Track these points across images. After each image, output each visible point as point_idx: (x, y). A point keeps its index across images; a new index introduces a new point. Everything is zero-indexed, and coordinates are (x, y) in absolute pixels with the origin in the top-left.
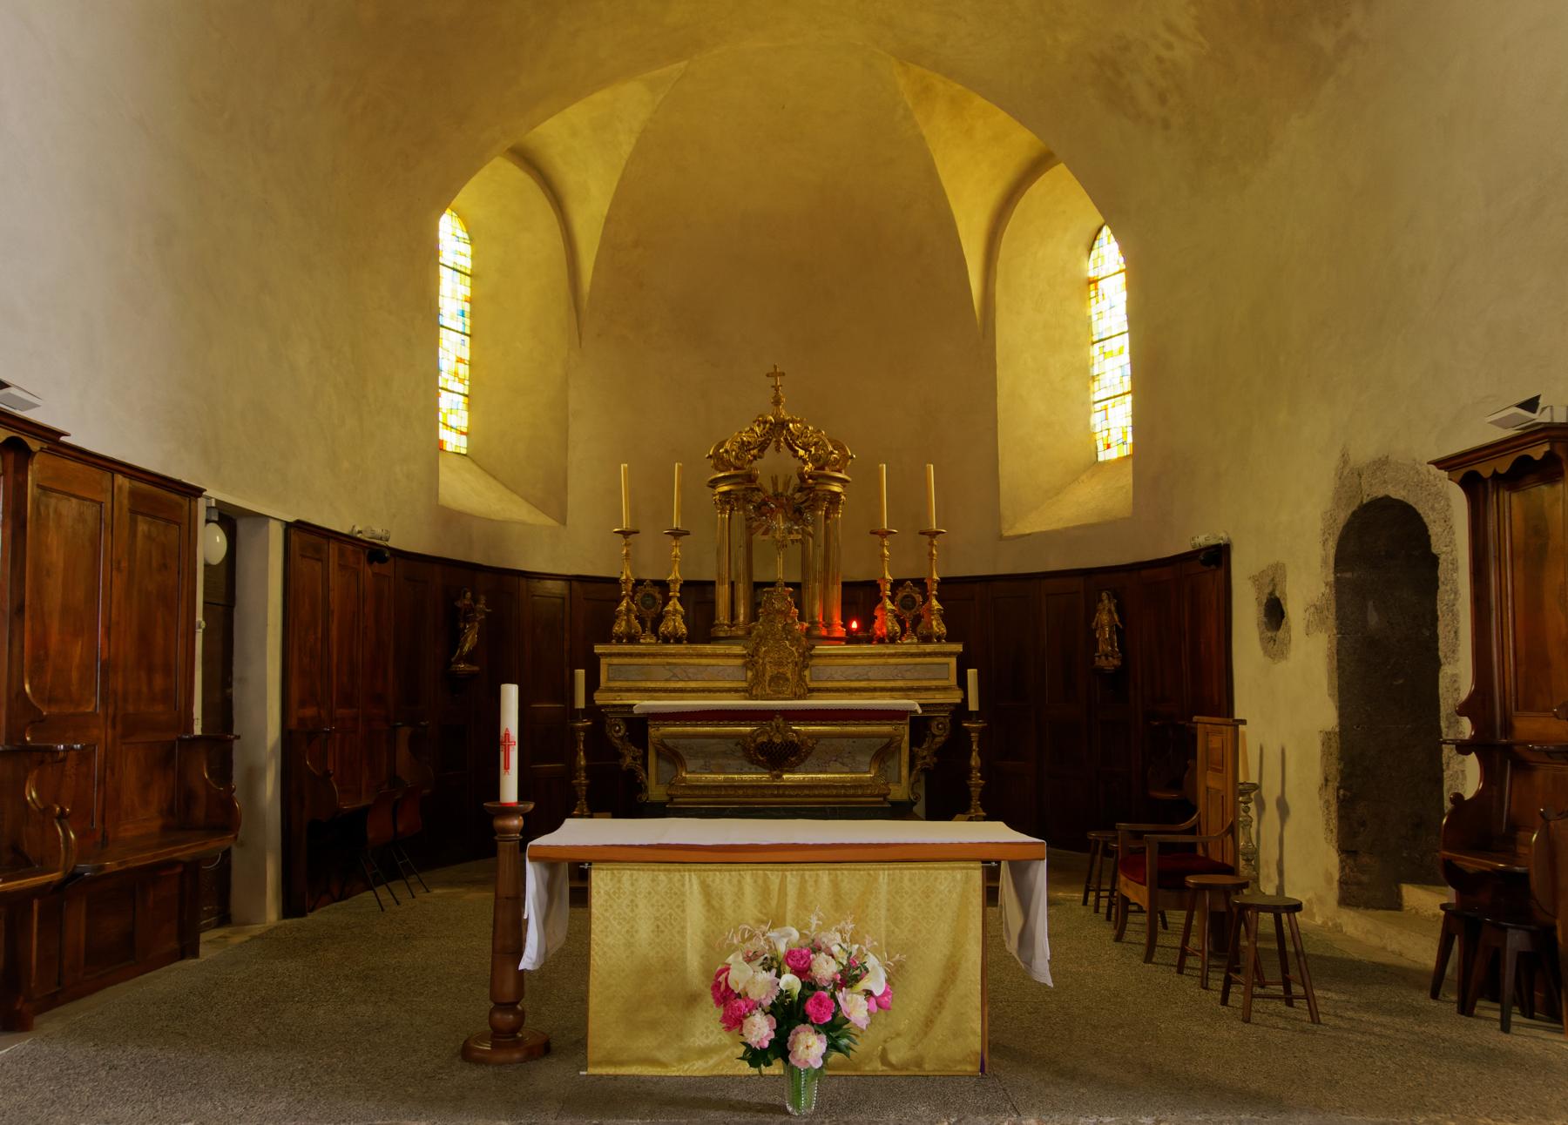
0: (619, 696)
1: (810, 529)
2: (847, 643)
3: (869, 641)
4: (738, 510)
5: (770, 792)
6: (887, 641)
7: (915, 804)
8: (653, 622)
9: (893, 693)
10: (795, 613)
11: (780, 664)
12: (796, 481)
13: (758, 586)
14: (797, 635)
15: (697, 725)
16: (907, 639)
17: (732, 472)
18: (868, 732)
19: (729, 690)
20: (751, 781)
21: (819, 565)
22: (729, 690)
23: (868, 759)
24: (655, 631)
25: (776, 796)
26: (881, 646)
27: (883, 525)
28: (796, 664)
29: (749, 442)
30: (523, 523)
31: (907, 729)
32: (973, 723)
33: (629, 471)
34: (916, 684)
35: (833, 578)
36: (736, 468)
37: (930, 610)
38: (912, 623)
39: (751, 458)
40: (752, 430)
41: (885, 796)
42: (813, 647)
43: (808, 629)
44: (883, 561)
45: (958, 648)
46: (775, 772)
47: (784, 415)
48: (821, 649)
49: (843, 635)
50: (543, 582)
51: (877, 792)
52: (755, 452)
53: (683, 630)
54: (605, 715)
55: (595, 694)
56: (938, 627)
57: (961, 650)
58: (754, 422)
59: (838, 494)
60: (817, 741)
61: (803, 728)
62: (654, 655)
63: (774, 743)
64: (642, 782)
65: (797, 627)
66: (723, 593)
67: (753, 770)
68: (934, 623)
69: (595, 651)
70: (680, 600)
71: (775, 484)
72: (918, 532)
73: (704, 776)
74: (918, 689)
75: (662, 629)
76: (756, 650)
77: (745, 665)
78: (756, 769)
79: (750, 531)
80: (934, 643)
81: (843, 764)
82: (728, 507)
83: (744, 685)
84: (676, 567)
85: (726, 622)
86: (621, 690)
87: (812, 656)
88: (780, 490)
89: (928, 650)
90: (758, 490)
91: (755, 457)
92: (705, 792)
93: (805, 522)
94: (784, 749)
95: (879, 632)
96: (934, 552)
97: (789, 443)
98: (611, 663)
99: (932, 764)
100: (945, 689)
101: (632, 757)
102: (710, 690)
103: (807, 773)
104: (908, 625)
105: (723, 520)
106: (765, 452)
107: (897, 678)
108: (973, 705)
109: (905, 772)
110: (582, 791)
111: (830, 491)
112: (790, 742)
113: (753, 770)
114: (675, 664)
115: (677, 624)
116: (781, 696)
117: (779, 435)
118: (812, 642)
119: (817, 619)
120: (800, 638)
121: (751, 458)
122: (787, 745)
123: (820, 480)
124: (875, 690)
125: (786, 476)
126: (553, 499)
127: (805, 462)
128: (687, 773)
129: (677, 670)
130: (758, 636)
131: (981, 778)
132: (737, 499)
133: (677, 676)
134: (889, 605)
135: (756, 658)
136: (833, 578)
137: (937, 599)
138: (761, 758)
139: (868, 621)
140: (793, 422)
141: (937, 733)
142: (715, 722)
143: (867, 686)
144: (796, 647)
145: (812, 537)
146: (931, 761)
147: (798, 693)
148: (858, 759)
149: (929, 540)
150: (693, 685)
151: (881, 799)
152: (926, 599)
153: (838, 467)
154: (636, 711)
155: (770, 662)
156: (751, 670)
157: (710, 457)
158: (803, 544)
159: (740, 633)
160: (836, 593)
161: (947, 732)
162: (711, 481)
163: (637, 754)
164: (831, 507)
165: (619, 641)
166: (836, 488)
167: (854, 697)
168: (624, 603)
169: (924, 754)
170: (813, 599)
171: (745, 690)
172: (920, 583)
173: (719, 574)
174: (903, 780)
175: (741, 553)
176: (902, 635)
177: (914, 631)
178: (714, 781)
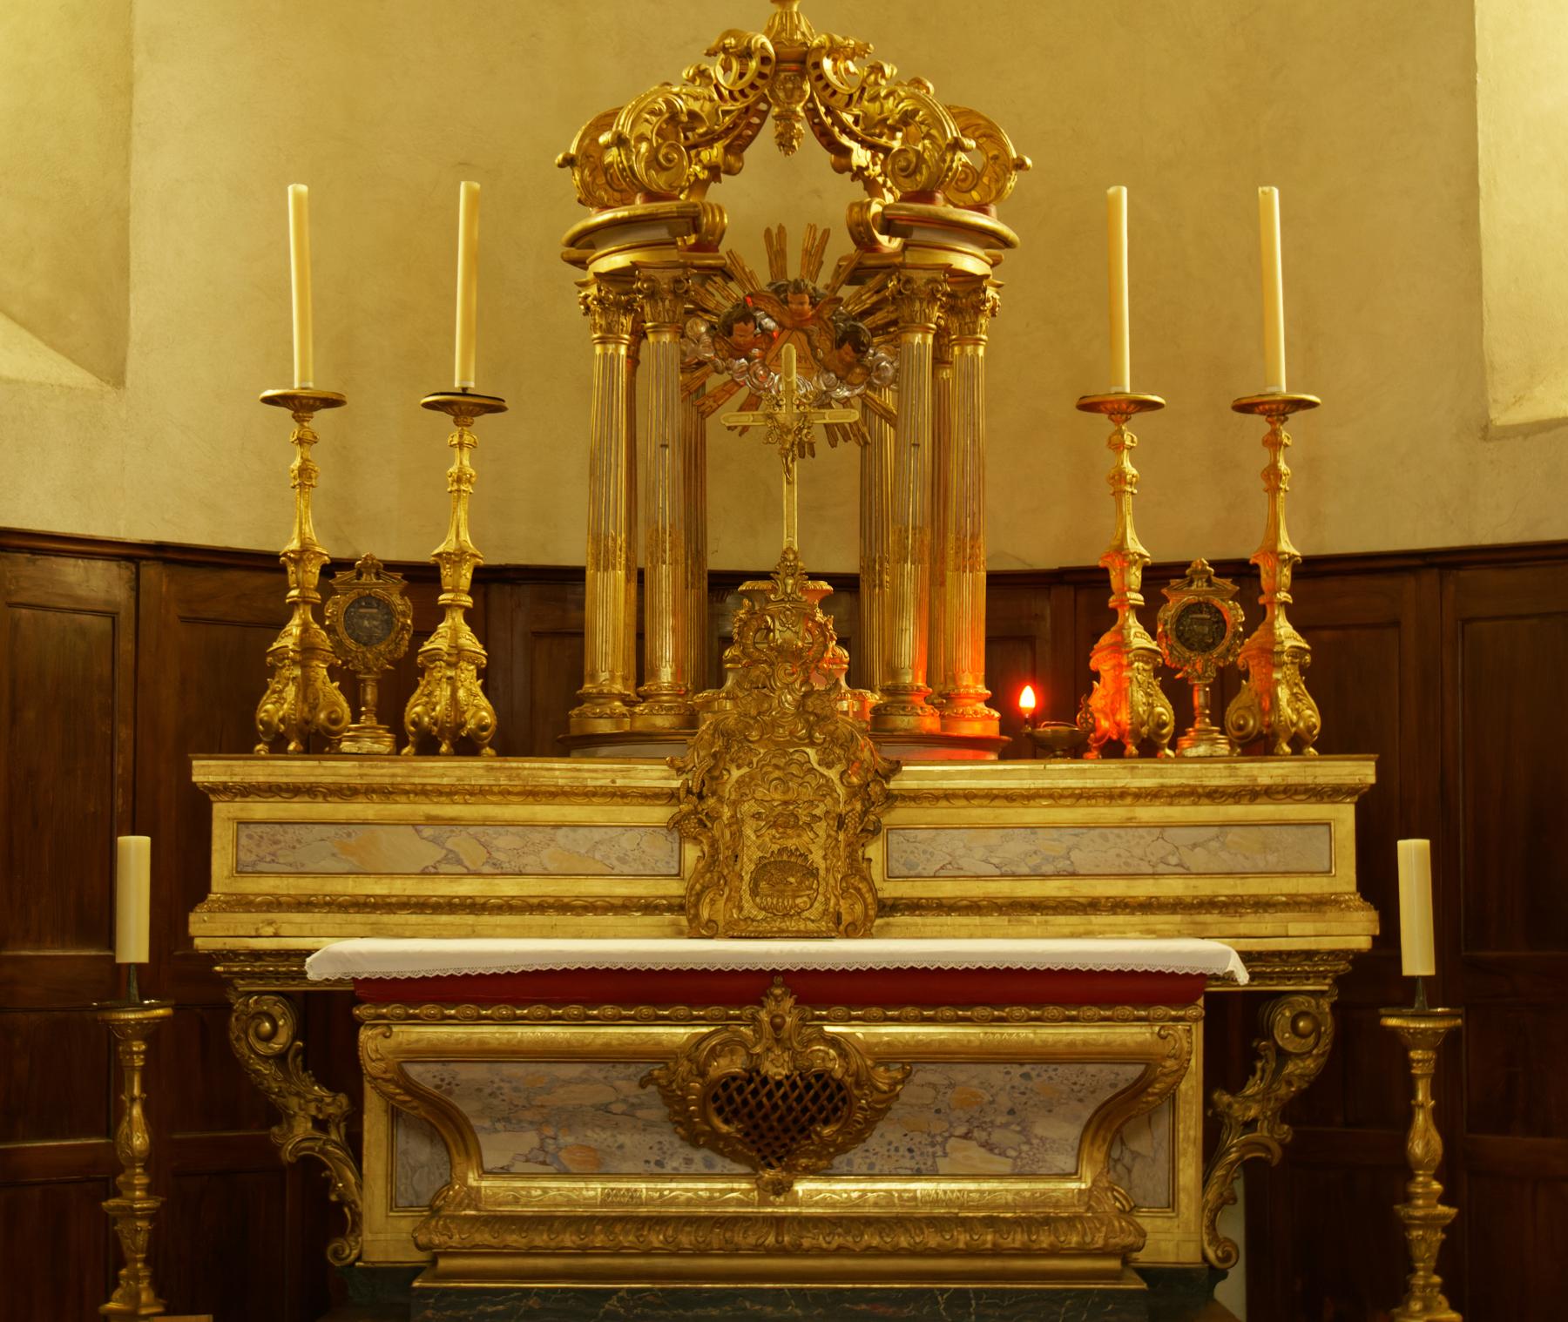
0: (270, 923)
1: (888, 398)
2: (1004, 756)
3: (1075, 749)
4: (656, 330)
5: (752, 1240)
6: (1132, 749)
7: (1223, 1275)
9: (1152, 918)
10: (836, 660)
11: (785, 821)
12: (842, 247)
13: (723, 583)
14: (843, 729)
15: (514, 1020)
16: (1196, 743)
17: (639, 206)
18: (1072, 1044)
19: (624, 906)
20: (689, 1202)
21: (915, 504)
22: (624, 906)
23: (1073, 1132)
24: (391, 715)
25: (770, 1253)
26: (1113, 766)
27: (1120, 382)
28: (841, 822)
29: (693, 115)
31: (1198, 1031)
32: (1415, 1016)
33: (315, 210)
34: (1224, 888)
35: (960, 549)
36: (651, 196)
37: (1269, 654)
39: (703, 175)
40: (702, 74)
41: (1124, 1254)
42: (895, 768)
43: (877, 710)
44: (1118, 494)
45: (1361, 771)
46: (768, 1175)
48: (918, 774)
49: (993, 729)
50: (43, 562)
51: (1100, 1242)
52: (714, 153)
53: (480, 711)
54: (225, 982)
55: (192, 917)
57: (1372, 780)
58: (711, 53)
59: (974, 283)
60: (908, 1075)
61: (859, 1031)
62: (385, 792)
63: (765, 1081)
64: (342, 1203)
65: (844, 705)
67: (698, 1166)
68: (1283, 693)
69: (194, 779)
70: (469, 616)
71: (777, 255)
72: (1230, 404)
73: (537, 1187)
74: (1232, 906)
75: (415, 709)
76: (713, 776)
77: (675, 825)
78: (709, 1164)
79: (698, 403)
80: (1283, 758)
81: (988, 1146)
82: (627, 322)
83: (675, 888)
84: (462, 514)
85: (618, 687)
86: (276, 904)
87: (891, 798)
88: (793, 273)
89: (1264, 780)
90: (728, 276)
91: (715, 172)
92: (541, 1239)
93: (871, 370)
94: (799, 1099)
95: (1105, 724)
96: (1283, 466)
97: (822, 123)
98: (244, 815)
99: (1275, 1147)
100: (1318, 904)
101: (315, 1120)
102: (563, 906)
103: (872, 1176)
104: (1199, 699)
105: (609, 361)
106: (747, 154)
107: (1161, 868)
108: (1417, 958)
109: (1189, 1171)
110: (137, 1236)
111: (948, 269)
112: (819, 1076)
113: (698, 1166)
114: (452, 822)
115: (461, 693)
116: (791, 925)
117: (790, 95)
118: (892, 752)
119: (908, 679)
120: (853, 738)
121: (703, 175)
122: (808, 1087)
123: (917, 236)
124: (1092, 906)
125: (813, 228)
127: (872, 187)
128: (485, 1173)
129: (459, 842)
130: (719, 731)
131: (1444, 1199)
132: (652, 295)
133: (459, 862)
134: (1138, 636)
135: (711, 801)
136: (960, 549)
137: (1290, 619)
138: (725, 1128)
140: (834, 51)
141: (1290, 1048)
142: (575, 1010)
143: (1066, 893)
144: (839, 768)
145: (894, 426)
146: (1273, 1136)
147: (846, 918)
148: (1039, 1130)
149: (1268, 428)
150: (508, 888)
151: (1114, 1264)
152: (1257, 616)
153: (975, 195)
154: (315, 970)
155: (757, 816)
156: (696, 840)
157: (569, 161)
158: (865, 444)
159: (663, 722)
161: (1326, 1041)
162: (573, 242)
163: (331, 1110)
164: (954, 324)
165: (278, 746)
166: (971, 261)
167: (1024, 929)
168: (294, 628)
169: (1252, 1113)
170: (896, 611)
171: (676, 907)
172: (1241, 573)
173: (597, 538)
174: (1183, 1198)
175: (664, 468)
176: (1180, 730)
177: (1218, 718)
178: (570, 1202)
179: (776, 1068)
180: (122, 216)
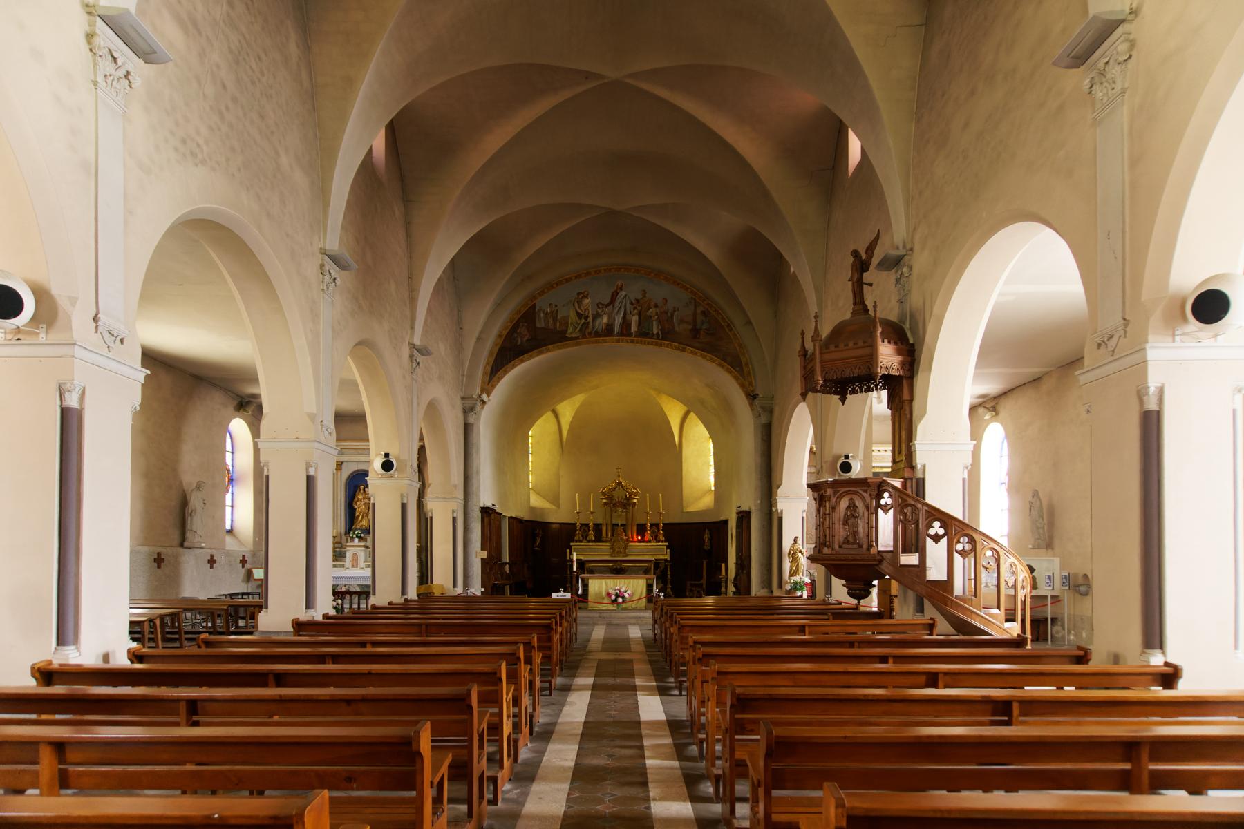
3: (643, 542)
8: (585, 537)
12: (624, 497)
18: (874, 695)
30: (548, 509)
31: (653, 565)
38: (656, 538)
45: (667, 544)
47: (621, 479)
48: (630, 544)
53: (593, 539)
56: (662, 538)
66: (604, 529)
75: (588, 539)
77: (610, 549)
79: (611, 511)
126: (555, 500)
134: (649, 532)
139: (643, 537)
152: (659, 530)
160: (635, 528)
166: (635, 501)
179: (619, 567)
180: (559, 493)
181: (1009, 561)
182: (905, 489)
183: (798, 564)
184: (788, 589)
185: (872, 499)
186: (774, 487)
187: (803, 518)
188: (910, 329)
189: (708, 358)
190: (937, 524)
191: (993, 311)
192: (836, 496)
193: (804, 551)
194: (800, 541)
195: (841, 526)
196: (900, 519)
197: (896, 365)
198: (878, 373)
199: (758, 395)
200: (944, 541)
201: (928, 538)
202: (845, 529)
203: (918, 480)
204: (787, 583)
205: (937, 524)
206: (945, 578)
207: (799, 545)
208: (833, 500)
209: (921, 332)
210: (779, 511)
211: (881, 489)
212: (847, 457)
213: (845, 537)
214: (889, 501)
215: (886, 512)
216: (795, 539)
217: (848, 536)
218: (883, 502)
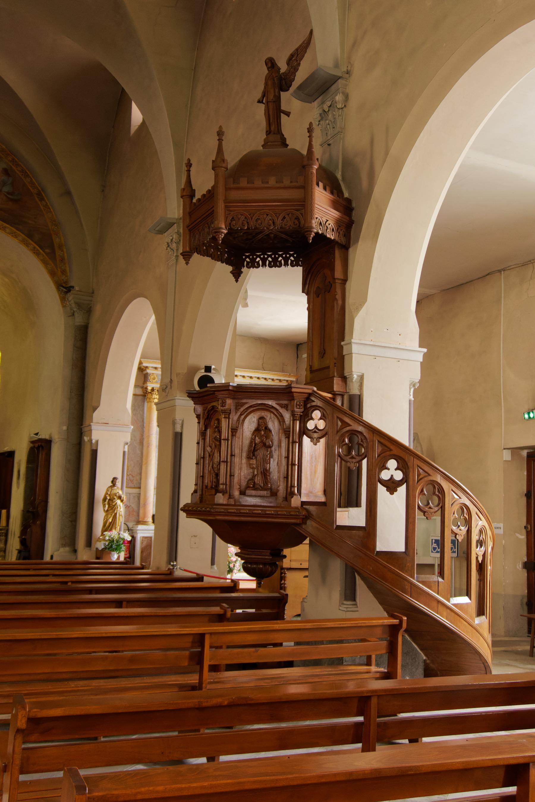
181: (480, 523)
182: (343, 406)
183: (116, 514)
184: (100, 549)
185: (294, 420)
186: (87, 411)
187: (124, 452)
188: (343, 179)
189: (8, 230)
190: (392, 464)
191: (461, 166)
192: (239, 414)
193: (124, 497)
194: (119, 483)
195: (244, 461)
196: (339, 452)
197: (331, 224)
198: (312, 228)
199: (73, 287)
200: (402, 490)
201: (379, 486)
202: (250, 464)
203: (351, 398)
204: (99, 540)
205: (392, 464)
206: (402, 549)
207: (118, 488)
208: (234, 417)
209: (365, 183)
210: (94, 441)
211: (309, 406)
212: (208, 369)
213: (250, 477)
214: (321, 425)
215: (315, 441)
216: (114, 481)
217: (254, 476)
218: (310, 425)
